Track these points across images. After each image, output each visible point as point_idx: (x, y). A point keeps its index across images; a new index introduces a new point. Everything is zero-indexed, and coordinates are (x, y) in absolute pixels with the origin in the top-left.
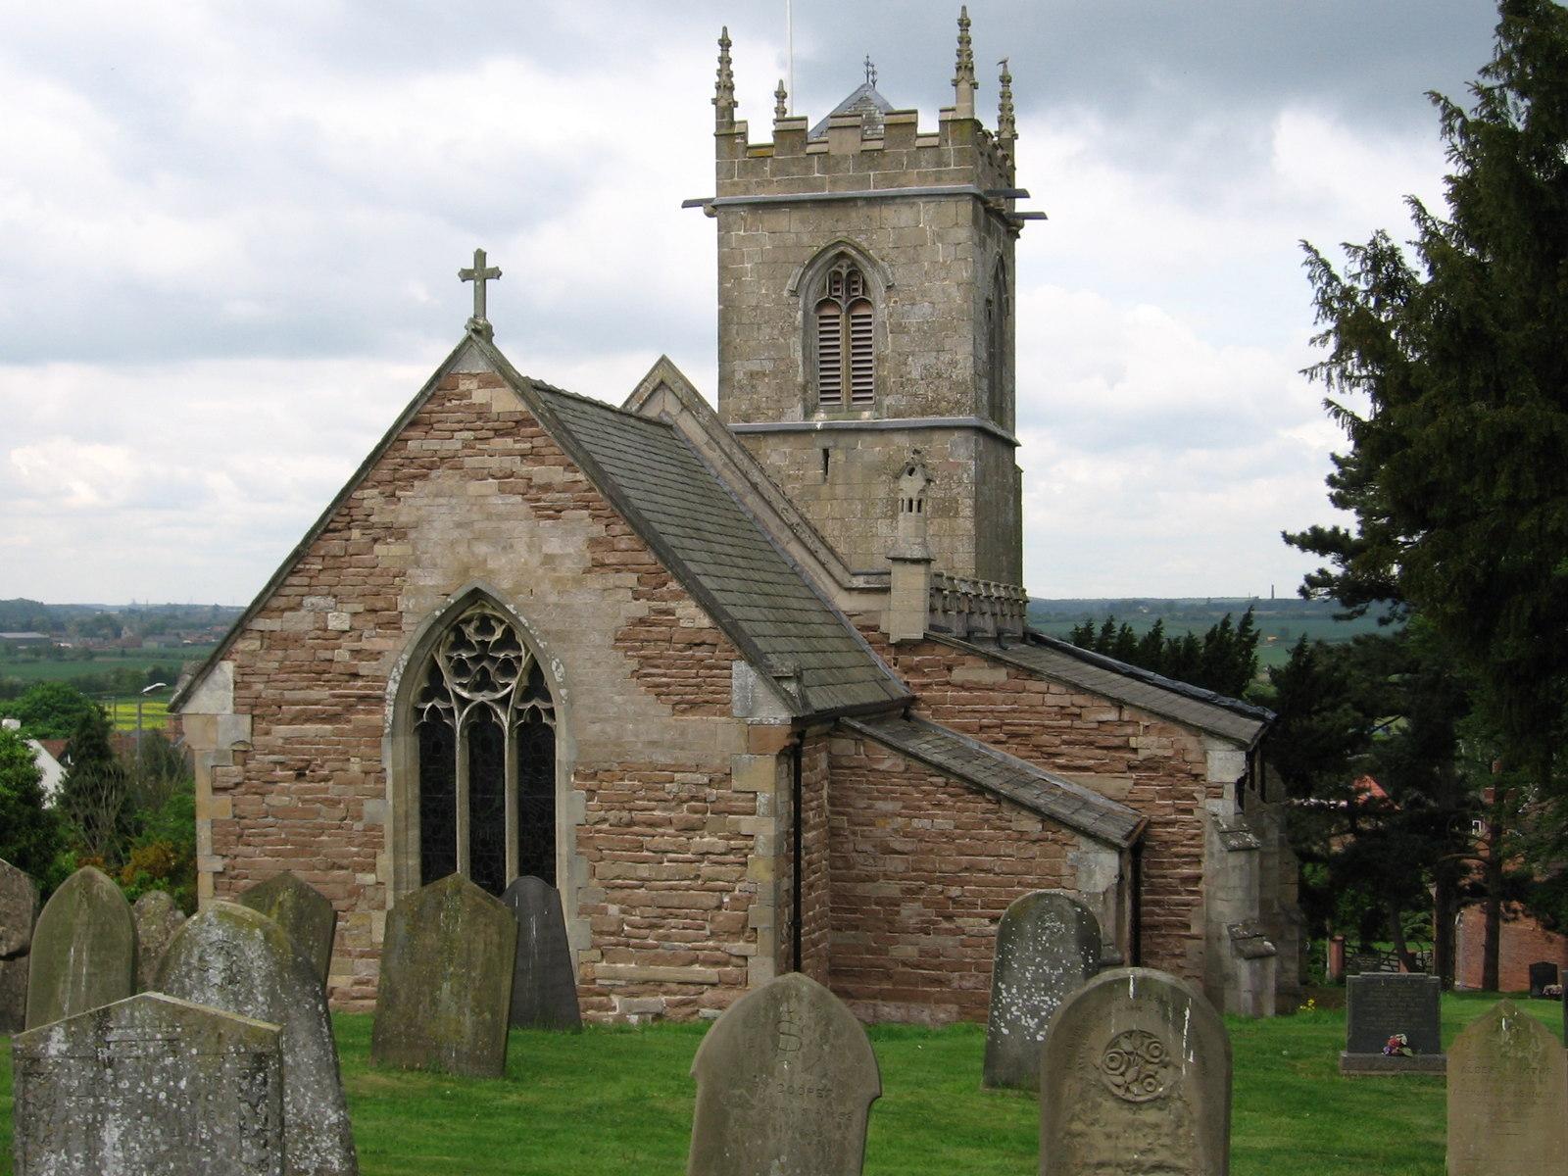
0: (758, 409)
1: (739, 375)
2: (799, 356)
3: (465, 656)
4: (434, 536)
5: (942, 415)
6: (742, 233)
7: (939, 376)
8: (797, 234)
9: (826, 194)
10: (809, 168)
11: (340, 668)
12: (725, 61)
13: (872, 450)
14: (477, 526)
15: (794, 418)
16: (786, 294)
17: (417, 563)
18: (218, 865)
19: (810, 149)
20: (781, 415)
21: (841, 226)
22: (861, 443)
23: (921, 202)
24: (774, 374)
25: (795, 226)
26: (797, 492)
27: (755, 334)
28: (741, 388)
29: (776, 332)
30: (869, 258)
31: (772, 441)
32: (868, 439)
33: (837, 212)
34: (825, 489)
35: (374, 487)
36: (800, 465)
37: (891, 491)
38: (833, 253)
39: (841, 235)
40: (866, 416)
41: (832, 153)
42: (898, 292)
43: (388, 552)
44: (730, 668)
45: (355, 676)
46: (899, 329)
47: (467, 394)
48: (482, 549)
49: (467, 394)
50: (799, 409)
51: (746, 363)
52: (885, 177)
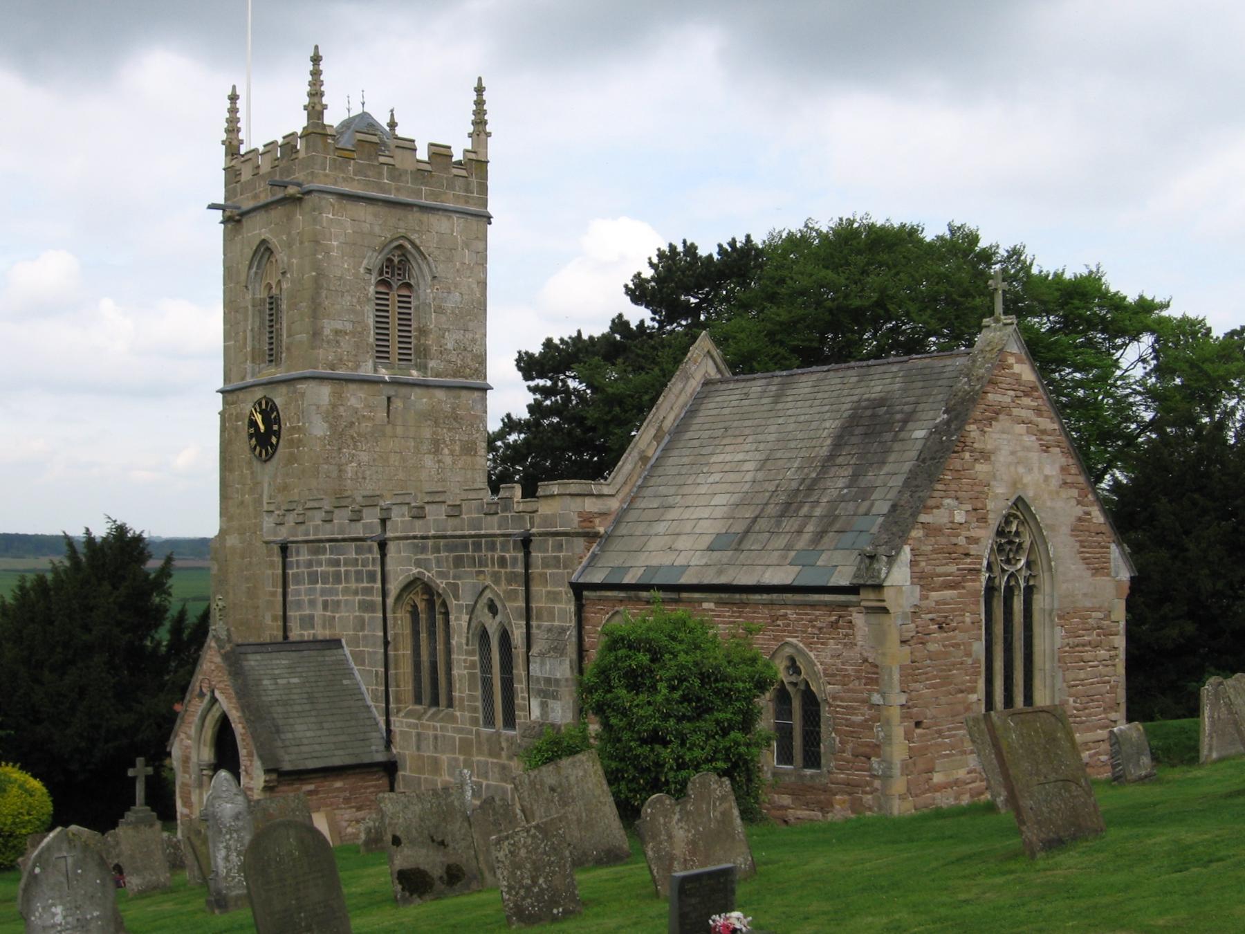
0: (341, 360)
1: (327, 332)
2: (371, 321)
3: (1003, 541)
4: (1002, 459)
5: (467, 378)
6: (330, 216)
7: (465, 349)
8: (371, 224)
9: (392, 197)
10: (380, 174)
11: (961, 550)
12: (316, 73)
13: (420, 400)
14: (1019, 454)
15: (367, 370)
16: (362, 270)
17: (994, 477)
18: (903, 699)
19: (382, 159)
20: (358, 367)
21: (401, 224)
22: (415, 394)
23: (455, 217)
24: (353, 334)
25: (369, 218)
26: (369, 429)
27: (339, 299)
28: (328, 342)
29: (355, 300)
30: (421, 253)
31: (352, 387)
32: (418, 391)
33: (399, 212)
34: (389, 429)
35: (973, 423)
36: (372, 408)
37: (434, 433)
38: (396, 244)
39: (402, 231)
40: (415, 374)
41: (397, 166)
42: (440, 281)
43: (981, 468)
44: (1109, 548)
45: (967, 555)
46: (440, 310)
47: (1011, 367)
48: (1021, 470)
49: (1011, 367)
50: (370, 364)
51: (332, 322)
52: (432, 193)
